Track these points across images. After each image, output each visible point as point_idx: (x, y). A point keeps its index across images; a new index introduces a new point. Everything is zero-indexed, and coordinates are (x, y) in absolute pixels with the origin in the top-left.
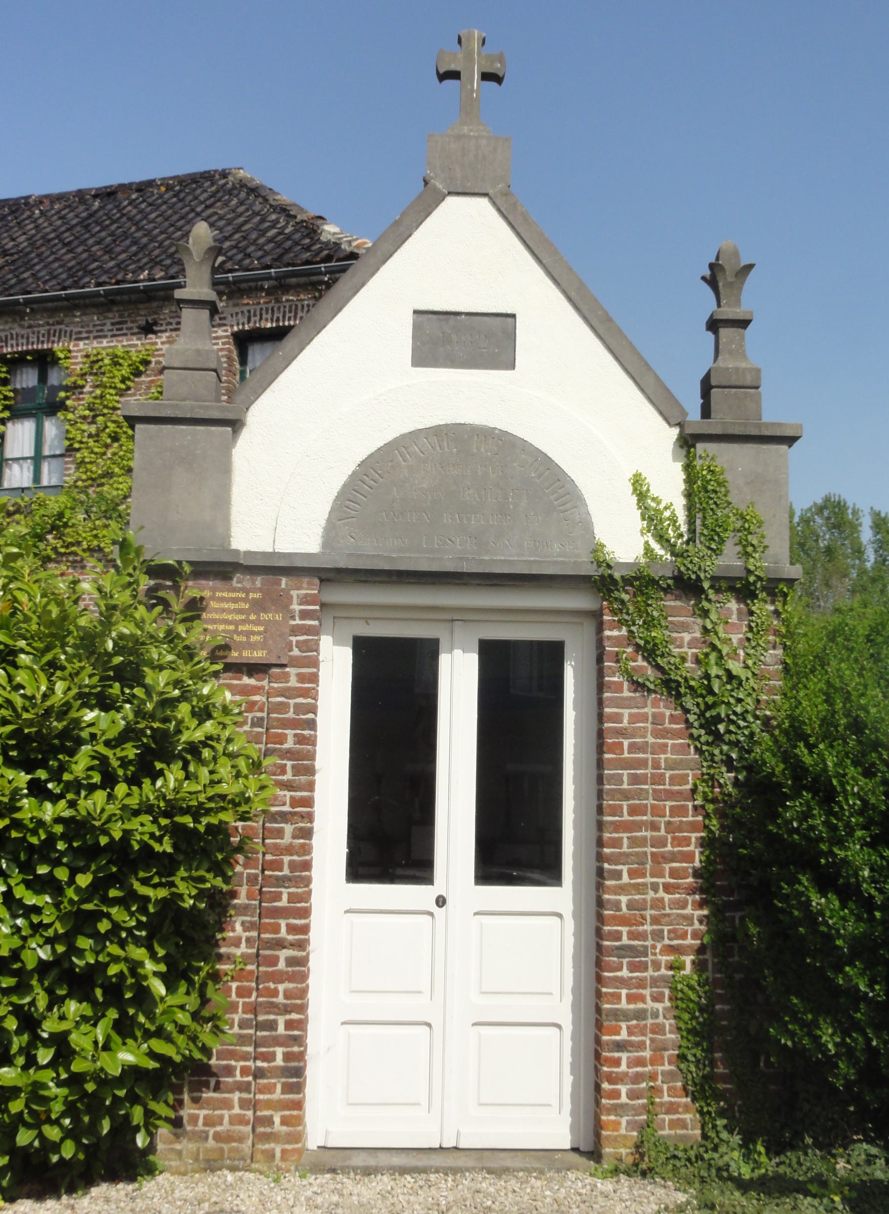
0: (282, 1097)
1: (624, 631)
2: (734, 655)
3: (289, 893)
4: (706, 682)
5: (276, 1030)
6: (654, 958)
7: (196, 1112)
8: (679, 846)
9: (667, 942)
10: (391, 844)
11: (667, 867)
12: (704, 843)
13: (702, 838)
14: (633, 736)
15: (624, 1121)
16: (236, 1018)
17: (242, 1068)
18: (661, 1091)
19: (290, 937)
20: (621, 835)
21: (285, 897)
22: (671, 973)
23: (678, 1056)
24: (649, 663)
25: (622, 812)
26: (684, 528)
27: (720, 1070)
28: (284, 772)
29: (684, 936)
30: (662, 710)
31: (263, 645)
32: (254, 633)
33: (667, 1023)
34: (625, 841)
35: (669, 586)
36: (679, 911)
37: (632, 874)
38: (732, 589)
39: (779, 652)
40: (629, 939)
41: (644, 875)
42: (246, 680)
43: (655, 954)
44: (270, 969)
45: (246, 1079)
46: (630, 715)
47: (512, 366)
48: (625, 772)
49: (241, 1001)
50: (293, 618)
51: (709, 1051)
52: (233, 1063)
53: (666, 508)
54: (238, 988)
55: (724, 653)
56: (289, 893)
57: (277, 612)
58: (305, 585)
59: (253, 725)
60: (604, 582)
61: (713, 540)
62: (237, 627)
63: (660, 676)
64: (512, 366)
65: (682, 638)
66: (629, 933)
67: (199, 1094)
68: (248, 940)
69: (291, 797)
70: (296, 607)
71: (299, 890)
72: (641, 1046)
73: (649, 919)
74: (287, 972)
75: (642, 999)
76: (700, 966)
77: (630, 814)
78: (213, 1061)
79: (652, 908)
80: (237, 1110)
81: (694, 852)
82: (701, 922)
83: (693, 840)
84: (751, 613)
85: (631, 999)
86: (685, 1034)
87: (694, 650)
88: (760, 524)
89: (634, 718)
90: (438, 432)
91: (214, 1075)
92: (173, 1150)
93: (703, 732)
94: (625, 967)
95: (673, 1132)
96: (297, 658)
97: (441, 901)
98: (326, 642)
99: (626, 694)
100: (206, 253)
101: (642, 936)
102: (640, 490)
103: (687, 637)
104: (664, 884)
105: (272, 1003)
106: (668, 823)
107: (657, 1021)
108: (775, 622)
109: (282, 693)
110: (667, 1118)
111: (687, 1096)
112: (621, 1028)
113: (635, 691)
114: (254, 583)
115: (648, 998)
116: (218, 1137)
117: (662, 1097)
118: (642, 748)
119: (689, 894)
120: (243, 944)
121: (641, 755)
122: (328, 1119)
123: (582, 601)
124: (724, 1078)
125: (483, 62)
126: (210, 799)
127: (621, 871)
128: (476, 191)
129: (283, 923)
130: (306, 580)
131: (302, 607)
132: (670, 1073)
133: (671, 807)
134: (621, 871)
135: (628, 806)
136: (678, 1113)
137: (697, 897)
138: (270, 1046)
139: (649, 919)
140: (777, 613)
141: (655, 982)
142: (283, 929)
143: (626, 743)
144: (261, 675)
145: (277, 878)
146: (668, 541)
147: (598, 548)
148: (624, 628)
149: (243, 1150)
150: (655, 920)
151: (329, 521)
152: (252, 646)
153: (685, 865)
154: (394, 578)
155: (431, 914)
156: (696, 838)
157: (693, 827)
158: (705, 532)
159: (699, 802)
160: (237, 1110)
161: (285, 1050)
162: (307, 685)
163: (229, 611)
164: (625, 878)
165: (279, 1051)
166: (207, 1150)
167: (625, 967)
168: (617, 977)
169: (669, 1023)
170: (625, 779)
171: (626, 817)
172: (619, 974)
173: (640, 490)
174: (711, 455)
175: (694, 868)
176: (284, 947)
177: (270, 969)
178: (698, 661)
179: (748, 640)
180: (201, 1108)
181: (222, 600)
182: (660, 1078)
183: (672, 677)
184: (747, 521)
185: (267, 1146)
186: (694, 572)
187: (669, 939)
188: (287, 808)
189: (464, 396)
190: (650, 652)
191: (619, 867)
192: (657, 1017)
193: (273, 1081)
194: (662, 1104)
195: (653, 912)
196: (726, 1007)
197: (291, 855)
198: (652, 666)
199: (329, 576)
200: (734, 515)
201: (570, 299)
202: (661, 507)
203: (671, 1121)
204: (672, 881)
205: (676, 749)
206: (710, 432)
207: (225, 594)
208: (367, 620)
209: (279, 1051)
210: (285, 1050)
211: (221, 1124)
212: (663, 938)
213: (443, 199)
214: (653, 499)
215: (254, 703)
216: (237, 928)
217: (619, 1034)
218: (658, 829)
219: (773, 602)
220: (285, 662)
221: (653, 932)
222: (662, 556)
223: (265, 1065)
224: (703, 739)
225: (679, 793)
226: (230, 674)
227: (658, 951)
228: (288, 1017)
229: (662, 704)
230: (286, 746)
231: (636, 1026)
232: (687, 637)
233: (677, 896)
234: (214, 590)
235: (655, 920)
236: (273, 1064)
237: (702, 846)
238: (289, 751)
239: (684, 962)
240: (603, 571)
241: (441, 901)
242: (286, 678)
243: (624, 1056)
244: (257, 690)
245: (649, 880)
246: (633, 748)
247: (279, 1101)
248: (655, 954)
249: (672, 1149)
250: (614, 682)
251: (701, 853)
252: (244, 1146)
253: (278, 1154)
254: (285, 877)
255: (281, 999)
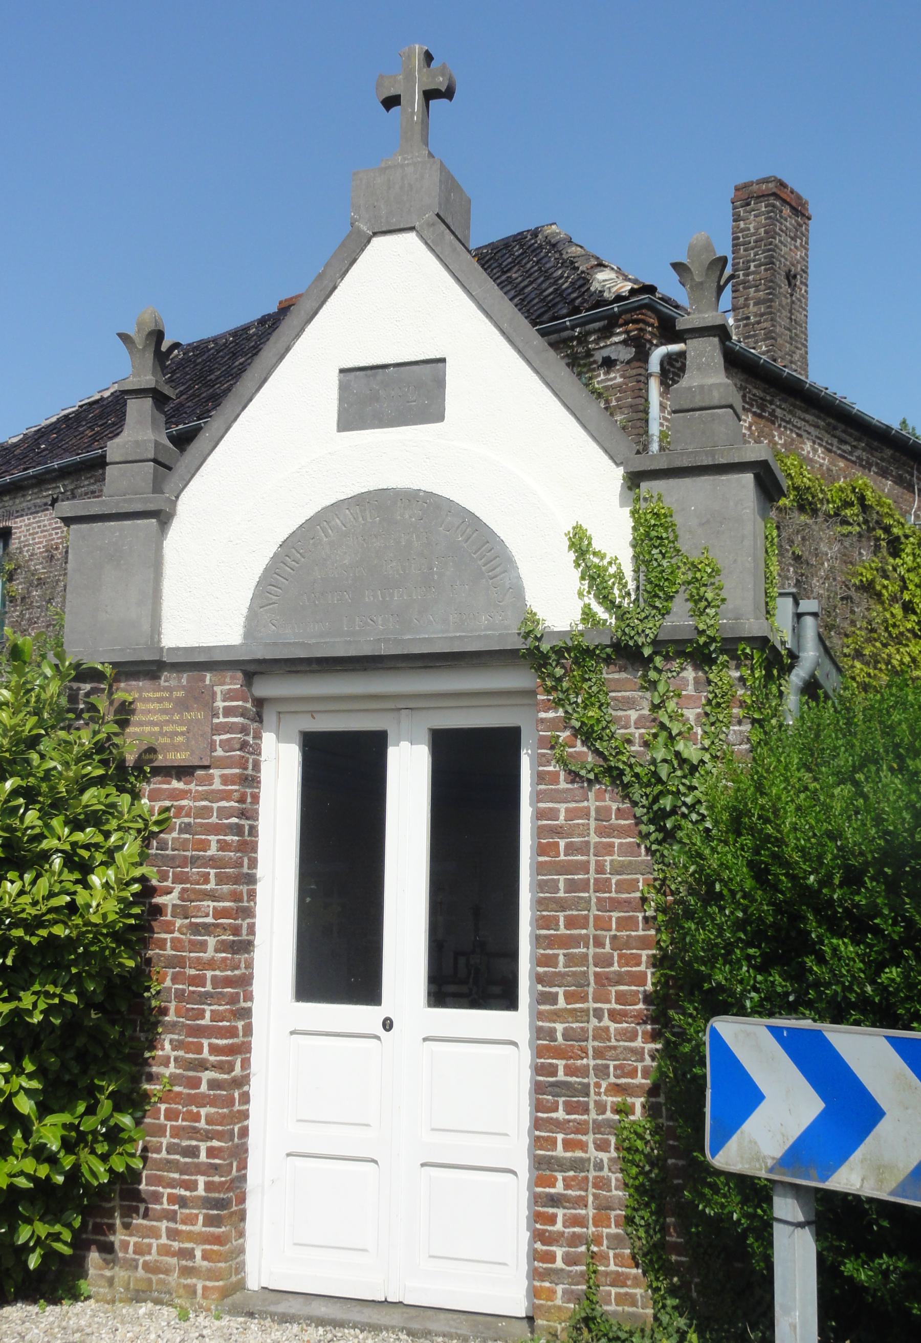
0: (204, 1229)
1: (561, 713)
2: (687, 734)
3: (212, 1011)
4: (653, 768)
5: (198, 1157)
6: (597, 1098)
7: (127, 1238)
8: (627, 965)
9: (612, 1079)
10: (339, 961)
11: (613, 990)
12: (657, 963)
13: (654, 956)
14: (570, 835)
15: (559, 1289)
16: (165, 1141)
17: (169, 1195)
18: (608, 1258)
19: (212, 1058)
20: (556, 951)
21: (208, 1015)
22: (617, 1117)
23: (626, 1217)
24: (589, 748)
25: (557, 924)
26: (631, 586)
27: (673, 1238)
28: (207, 881)
29: (633, 1073)
30: (608, 803)
31: (187, 746)
32: (177, 734)
33: (613, 1177)
34: (561, 959)
35: (608, 655)
36: (626, 1044)
37: (569, 997)
38: (680, 654)
39: (746, 727)
40: (566, 1075)
41: (584, 999)
42: (176, 784)
43: (599, 1094)
44: (193, 1092)
45: (172, 1208)
46: (567, 810)
47: (440, 417)
48: (562, 878)
49: (169, 1123)
50: (216, 715)
51: (660, 1213)
52: (161, 1189)
53: (610, 563)
54: (166, 1110)
55: (674, 733)
56: (212, 1011)
57: (198, 710)
58: (228, 680)
59: (181, 831)
60: (536, 655)
61: (656, 596)
62: (161, 728)
63: (602, 763)
64: (440, 417)
65: (628, 717)
66: (566, 1067)
67: (129, 1220)
68: (176, 1059)
69: (214, 908)
70: (220, 704)
71: (221, 1008)
72: (581, 1202)
73: (591, 1052)
74: (209, 1095)
75: (583, 1146)
76: (652, 1110)
77: (566, 928)
78: (143, 1187)
79: (594, 1039)
80: (164, 1240)
81: (645, 973)
82: (653, 1058)
83: (644, 959)
84: (709, 682)
85: (568, 1145)
86: (632, 1190)
87: (643, 731)
88: (716, 572)
89: (572, 814)
90: (360, 500)
91: (143, 1201)
92: (102, 1275)
93: (652, 828)
94: (561, 1108)
95: (620, 1309)
96: (220, 758)
97: (388, 1025)
98: (268, 739)
99: (563, 785)
100: (147, 339)
101: (583, 1072)
102: (580, 545)
103: (633, 715)
104: (609, 1010)
105: (194, 1128)
106: (614, 938)
107: (601, 1174)
108: (740, 692)
109: (205, 796)
110: (613, 1290)
111: (637, 1266)
112: (556, 1179)
113: (573, 782)
114: (180, 680)
115: (591, 1146)
116: (146, 1265)
117: (608, 1266)
118: (583, 848)
119: (638, 1024)
120: (172, 1064)
121: (579, 858)
122: (272, 1256)
123: (519, 679)
124: (676, 1249)
125: (425, 79)
126: (50, 911)
127: (557, 994)
128: (402, 226)
129: (205, 1043)
130: (229, 674)
131: (227, 704)
132: (616, 1236)
133: (618, 919)
134: (557, 994)
135: (565, 917)
136: (627, 1286)
137: (649, 1027)
138: (191, 1174)
139: (591, 1052)
140: (742, 679)
141: (598, 1127)
142: (206, 1049)
143: (562, 843)
144: (188, 778)
145: (200, 994)
146: (612, 602)
147: (531, 618)
148: (561, 710)
149: (169, 1283)
150: (599, 1053)
151: (250, 609)
152: (176, 748)
153: (634, 988)
154: (315, 667)
155: (378, 1038)
156: (648, 956)
157: (644, 943)
158: (649, 587)
159: (650, 913)
160: (164, 1240)
161: (207, 1179)
162: (230, 787)
163: (154, 712)
164: (562, 1003)
165: (201, 1180)
166: (137, 1280)
167: (561, 1108)
168: (552, 1119)
169: (615, 1178)
170: (561, 885)
171: (562, 930)
172: (554, 1115)
173: (580, 545)
174: (655, 495)
175: (645, 991)
176: (207, 1069)
177: (193, 1092)
178: (646, 744)
179: (707, 714)
180: (131, 1235)
181: (149, 700)
182: (605, 1242)
183: (612, 764)
184: (699, 570)
185: (189, 1281)
186: (631, 638)
187: (616, 1077)
188: (209, 920)
189: (394, 458)
190: (587, 734)
191: (554, 990)
192: (601, 1169)
193: (195, 1211)
194: (607, 1274)
195: (596, 1044)
196: (681, 1163)
197: (214, 970)
198: (593, 752)
199: (253, 670)
200: (685, 564)
201: (503, 333)
202: (605, 562)
203: (618, 1295)
204: (619, 1007)
205: (626, 850)
206: (653, 468)
207: (150, 695)
208: (312, 714)
209: (201, 1180)
210: (207, 1179)
211: (150, 1253)
212: (609, 1076)
213: (369, 242)
214: (595, 554)
215: (181, 808)
216: (166, 1048)
217: (554, 1186)
218: (603, 946)
219: (738, 667)
220: (207, 763)
221: (596, 1068)
222: (606, 620)
223: (188, 1193)
224: (653, 837)
225: (628, 902)
226: (159, 778)
227: (602, 1090)
228: (209, 1144)
229: (607, 796)
230: (209, 853)
231: (574, 1178)
232: (633, 715)
233: (625, 1025)
234: (140, 690)
235: (599, 1053)
236: (195, 1193)
237: (654, 966)
238: (212, 858)
239: (634, 1104)
240: (530, 643)
241: (388, 1025)
242: (210, 780)
243: (560, 1213)
244: (183, 794)
245: (592, 1005)
246: (570, 849)
247: (200, 1234)
248: (599, 1094)
249: (615, 1329)
250: (549, 772)
251: (653, 974)
252: (170, 1279)
253: (200, 1291)
254: (207, 993)
255: (202, 1124)
